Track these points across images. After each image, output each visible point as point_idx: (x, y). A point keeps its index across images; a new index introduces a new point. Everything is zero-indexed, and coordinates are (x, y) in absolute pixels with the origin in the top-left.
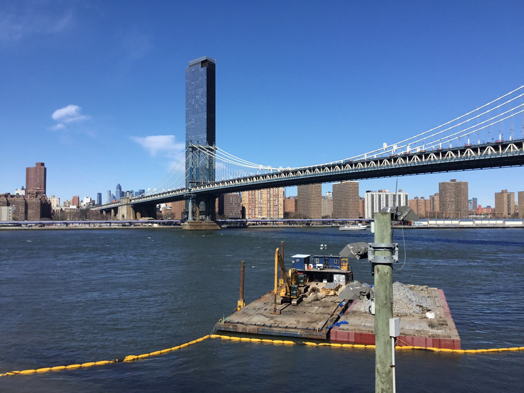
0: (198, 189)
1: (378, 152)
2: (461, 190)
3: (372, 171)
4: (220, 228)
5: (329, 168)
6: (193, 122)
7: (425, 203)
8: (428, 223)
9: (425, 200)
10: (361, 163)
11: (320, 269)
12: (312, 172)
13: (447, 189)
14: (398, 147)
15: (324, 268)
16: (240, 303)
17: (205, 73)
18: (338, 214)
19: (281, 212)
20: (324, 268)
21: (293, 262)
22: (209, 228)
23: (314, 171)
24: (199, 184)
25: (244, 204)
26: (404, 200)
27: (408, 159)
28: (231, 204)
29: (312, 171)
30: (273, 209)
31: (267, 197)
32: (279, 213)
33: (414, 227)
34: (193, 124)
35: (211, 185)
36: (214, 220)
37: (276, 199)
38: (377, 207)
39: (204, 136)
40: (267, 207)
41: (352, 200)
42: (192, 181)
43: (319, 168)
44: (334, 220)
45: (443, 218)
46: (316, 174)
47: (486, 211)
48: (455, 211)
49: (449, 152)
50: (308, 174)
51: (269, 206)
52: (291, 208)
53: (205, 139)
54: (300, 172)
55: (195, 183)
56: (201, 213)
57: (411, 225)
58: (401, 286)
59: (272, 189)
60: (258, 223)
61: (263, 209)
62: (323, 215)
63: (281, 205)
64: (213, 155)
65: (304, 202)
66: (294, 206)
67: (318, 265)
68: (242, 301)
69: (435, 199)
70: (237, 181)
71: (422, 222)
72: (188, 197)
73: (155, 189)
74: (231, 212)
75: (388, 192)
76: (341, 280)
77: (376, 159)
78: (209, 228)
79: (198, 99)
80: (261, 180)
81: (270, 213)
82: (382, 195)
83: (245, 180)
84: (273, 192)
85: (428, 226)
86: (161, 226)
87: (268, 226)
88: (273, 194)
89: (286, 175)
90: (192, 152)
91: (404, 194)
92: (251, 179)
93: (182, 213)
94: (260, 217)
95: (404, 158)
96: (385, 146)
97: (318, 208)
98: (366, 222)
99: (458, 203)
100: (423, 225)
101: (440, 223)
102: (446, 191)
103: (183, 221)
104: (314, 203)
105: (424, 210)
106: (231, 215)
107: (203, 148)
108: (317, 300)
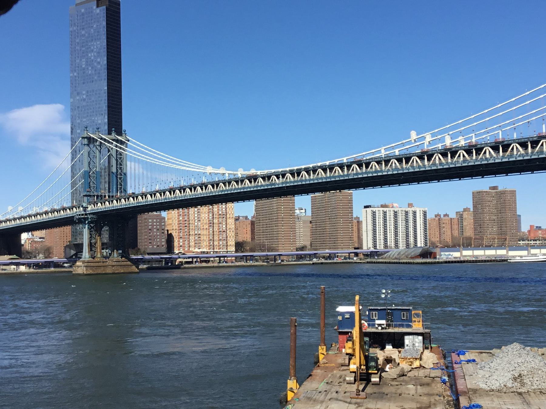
0: (100, 207)
1: (403, 145)
2: (505, 203)
3: (394, 174)
4: (137, 270)
5: (324, 170)
6: (84, 97)
7: (451, 224)
8: (461, 254)
9: (451, 219)
10: (376, 162)
11: (382, 328)
12: (296, 177)
13: (485, 201)
14: (432, 137)
15: (388, 326)
16: (292, 383)
17: (104, 17)
18: (321, 244)
19: (232, 242)
20: (388, 326)
21: (340, 318)
22: (118, 270)
23: (298, 176)
24: (101, 198)
25: (171, 230)
26: (422, 219)
27: (449, 155)
28: (150, 230)
29: (296, 175)
30: (219, 238)
31: (209, 218)
32: (228, 244)
33: (440, 261)
34: (84, 100)
35: (123, 200)
36: (126, 258)
37: (222, 221)
38: (382, 231)
39: (103, 120)
40: (209, 235)
41: (343, 220)
42: (88, 193)
43: (307, 171)
44: (317, 253)
45: (482, 246)
46: (288, 183)
47: (542, 234)
48: (498, 234)
49: (514, 144)
50: (288, 180)
51: (211, 232)
52: (246, 236)
53: (105, 123)
54: (275, 177)
55: (94, 196)
56: (104, 246)
57: (435, 258)
58: (522, 349)
59: (215, 206)
60: (195, 260)
61: (202, 237)
62: (299, 244)
63: (232, 231)
64: (123, 149)
65: (266, 225)
66: (249, 232)
67: (378, 322)
68: (295, 381)
69: (464, 217)
70: (168, 193)
71: (451, 253)
72: (83, 220)
73: (20, 208)
74: (150, 243)
75: (397, 207)
76: (417, 345)
77: (399, 155)
78: (118, 270)
79: (92, 58)
80: (210, 190)
81: (213, 243)
82: (388, 212)
83: (182, 191)
84: (218, 210)
85: (462, 259)
86: (32, 270)
87: (210, 264)
88: (218, 212)
89: (253, 183)
90: (88, 145)
91: (421, 210)
92: (193, 189)
93: (65, 247)
94: (197, 250)
95: (444, 154)
96: (414, 135)
97: (290, 234)
98: (364, 255)
99: (501, 224)
100: (454, 258)
101: (480, 253)
102: (483, 204)
103: (73, 259)
104: (283, 226)
105: (450, 233)
106: (150, 248)
107: (107, 139)
108: (403, 375)
